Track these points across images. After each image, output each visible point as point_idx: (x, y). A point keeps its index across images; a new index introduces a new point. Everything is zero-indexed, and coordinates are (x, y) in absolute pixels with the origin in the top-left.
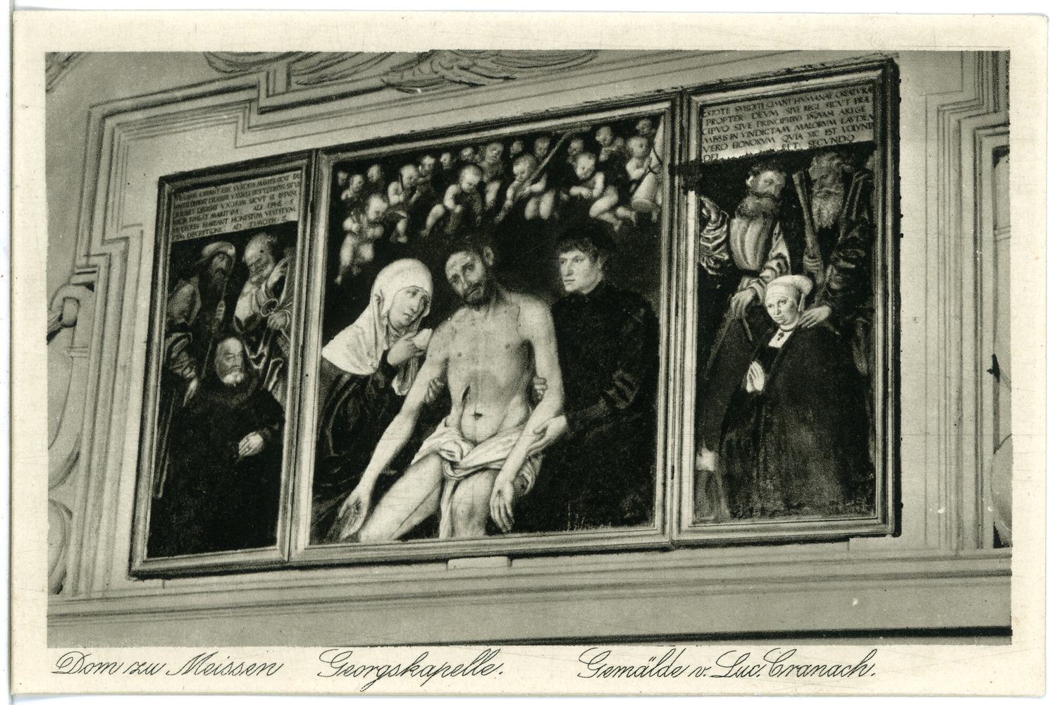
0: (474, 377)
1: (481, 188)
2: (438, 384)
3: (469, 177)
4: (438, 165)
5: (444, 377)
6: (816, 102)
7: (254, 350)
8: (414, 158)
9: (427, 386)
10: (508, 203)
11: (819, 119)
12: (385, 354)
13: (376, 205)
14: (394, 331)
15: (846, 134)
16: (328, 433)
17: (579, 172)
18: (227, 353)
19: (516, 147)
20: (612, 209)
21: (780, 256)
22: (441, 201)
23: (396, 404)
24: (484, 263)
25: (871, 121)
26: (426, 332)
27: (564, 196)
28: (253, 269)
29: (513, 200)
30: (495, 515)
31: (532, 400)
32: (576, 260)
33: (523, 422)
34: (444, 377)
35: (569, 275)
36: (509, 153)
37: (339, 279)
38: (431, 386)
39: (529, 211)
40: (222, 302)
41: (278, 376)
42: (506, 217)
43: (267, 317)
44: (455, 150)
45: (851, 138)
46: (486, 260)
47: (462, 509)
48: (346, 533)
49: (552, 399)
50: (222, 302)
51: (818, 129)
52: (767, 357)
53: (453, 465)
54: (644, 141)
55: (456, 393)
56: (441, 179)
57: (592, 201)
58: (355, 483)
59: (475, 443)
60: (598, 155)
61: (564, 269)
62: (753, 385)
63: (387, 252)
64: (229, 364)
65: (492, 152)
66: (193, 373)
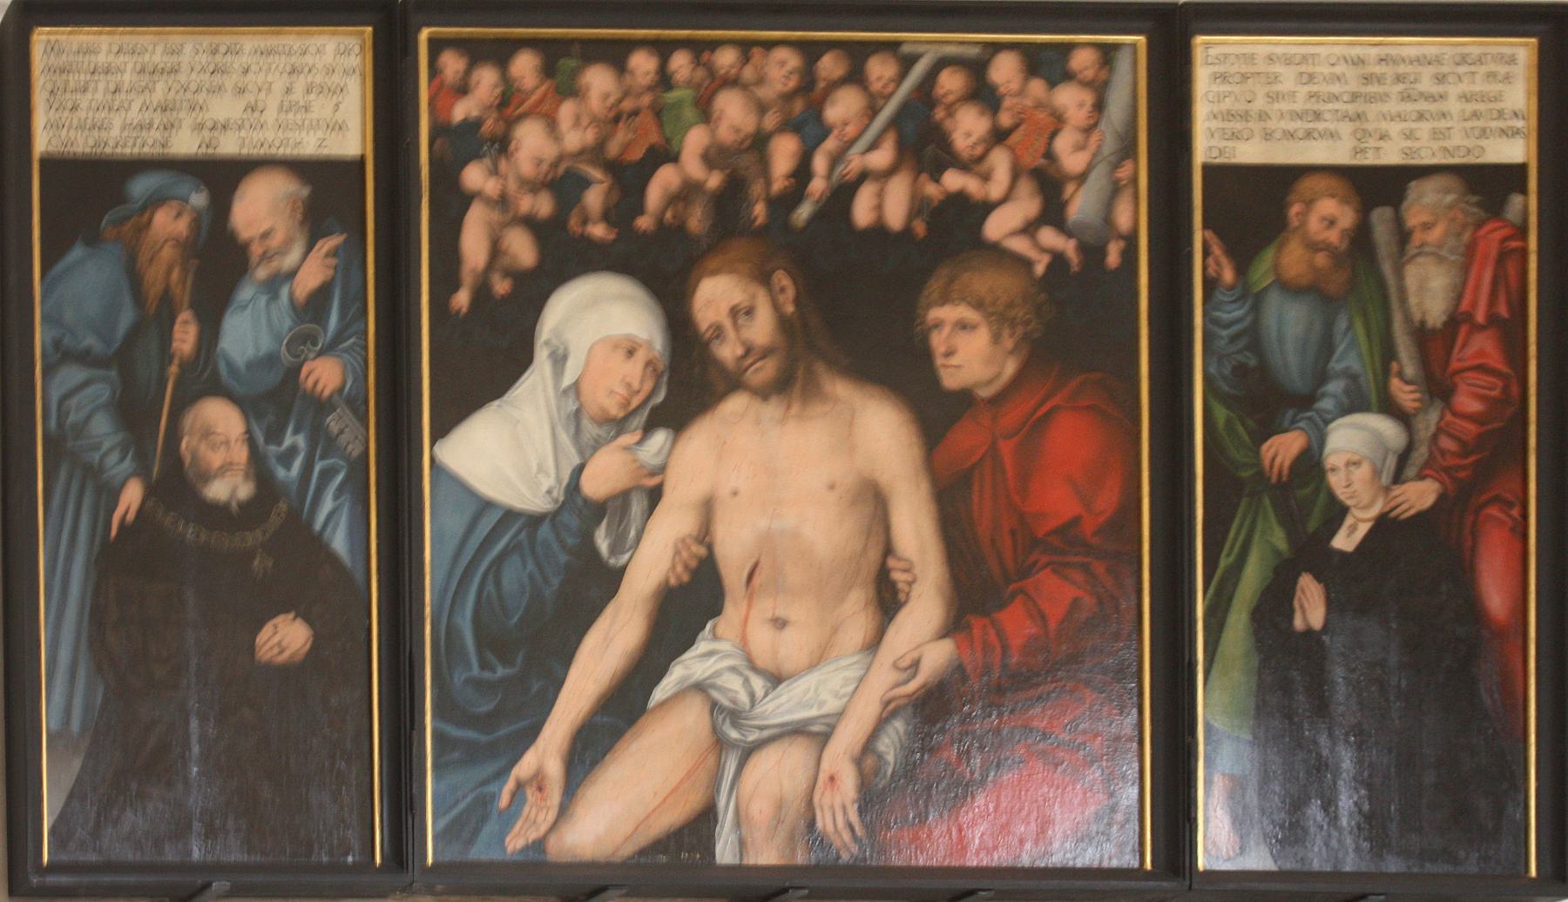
1: (759, 143)
3: (733, 112)
5: (705, 535)
7: (275, 435)
12: (579, 470)
19: (830, 66)
20: (1029, 229)
22: (673, 158)
23: (595, 584)
24: (776, 306)
26: (660, 438)
27: (931, 190)
28: (256, 250)
30: (824, 822)
31: (888, 599)
32: (963, 326)
34: (705, 535)
40: (185, 315)
41: (336, 498)
42: (817, 217)
46: (781, 298)
50: (185, 315)
53: (735, 716)
54: (1088, 98)
57: (988, 207)
59: (776, 679)
61: (938, 341)
63: (565, 257)
64: (216, 459)
66: (127, 465)
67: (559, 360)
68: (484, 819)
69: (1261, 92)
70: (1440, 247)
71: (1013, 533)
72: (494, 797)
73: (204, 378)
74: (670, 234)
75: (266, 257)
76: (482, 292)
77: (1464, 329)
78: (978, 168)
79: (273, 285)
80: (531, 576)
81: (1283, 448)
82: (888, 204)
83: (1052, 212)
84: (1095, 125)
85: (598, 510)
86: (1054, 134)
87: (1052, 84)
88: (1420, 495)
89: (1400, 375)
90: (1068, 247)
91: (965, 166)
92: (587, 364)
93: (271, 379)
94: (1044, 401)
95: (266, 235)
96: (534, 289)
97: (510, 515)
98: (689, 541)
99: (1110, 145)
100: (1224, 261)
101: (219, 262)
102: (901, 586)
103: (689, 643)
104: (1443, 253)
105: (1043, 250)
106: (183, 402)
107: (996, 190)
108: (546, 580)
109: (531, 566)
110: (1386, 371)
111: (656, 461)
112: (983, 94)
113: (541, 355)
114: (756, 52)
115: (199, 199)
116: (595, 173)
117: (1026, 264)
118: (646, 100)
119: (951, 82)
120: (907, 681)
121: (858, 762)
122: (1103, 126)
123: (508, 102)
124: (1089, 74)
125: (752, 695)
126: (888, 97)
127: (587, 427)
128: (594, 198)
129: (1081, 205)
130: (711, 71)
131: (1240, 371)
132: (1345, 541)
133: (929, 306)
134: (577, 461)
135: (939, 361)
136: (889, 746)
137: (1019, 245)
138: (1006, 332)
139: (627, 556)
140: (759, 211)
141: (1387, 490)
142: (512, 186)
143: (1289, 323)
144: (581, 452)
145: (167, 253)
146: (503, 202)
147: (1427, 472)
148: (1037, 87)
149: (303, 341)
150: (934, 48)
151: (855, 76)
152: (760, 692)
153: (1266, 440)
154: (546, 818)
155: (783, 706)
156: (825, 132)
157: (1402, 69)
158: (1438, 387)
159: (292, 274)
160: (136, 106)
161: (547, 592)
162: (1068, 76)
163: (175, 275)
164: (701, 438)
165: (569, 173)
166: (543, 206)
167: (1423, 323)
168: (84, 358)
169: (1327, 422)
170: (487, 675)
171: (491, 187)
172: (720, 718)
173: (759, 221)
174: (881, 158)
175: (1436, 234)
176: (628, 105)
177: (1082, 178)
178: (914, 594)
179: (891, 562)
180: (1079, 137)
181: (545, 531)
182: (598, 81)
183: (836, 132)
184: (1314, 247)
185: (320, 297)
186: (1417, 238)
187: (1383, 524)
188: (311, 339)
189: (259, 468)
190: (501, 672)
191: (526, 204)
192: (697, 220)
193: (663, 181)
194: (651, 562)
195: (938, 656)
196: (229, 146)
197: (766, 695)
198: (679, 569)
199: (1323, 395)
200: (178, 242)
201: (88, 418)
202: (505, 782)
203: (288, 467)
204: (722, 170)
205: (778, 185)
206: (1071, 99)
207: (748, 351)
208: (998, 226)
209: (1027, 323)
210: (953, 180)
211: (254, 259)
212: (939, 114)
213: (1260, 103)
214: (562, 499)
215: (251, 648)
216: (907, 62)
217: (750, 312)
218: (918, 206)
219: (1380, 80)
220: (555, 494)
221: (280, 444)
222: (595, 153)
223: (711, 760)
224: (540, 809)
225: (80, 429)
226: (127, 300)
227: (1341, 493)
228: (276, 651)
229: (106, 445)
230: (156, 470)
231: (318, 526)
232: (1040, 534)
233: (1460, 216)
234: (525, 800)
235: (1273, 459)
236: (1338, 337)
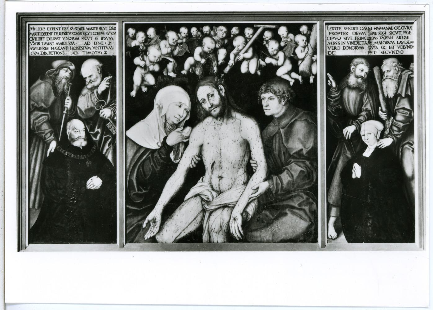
1: (215, 51)
2: (197, 158)
3: (208, 44)
4: (189, 33)
5: (200, 155)
6: (384, 30)
7: (92, 129)
8: (176, 28)
9: (191, 159)
11: (386, 40)
12: (165, 138)
13: (154, 53)
14: (170, 127)
15: (400, 50)
17: (270, 51)
19: (235, 30)
20: (289, 73)
21: (366, 110)
22: (192, 55)
23: (172, 168)
24: (220, 94)
26: (188, 129)
27: (262, 63)
28: (88, 80)
29: (234, 60)
30: (232, 231)
31: (250, 171)
32: (270, 98)
33: (246, 183)
34: (200, 155)
35: (267, 106)
36: (231, 34)
37: (133, 93)
38: (193, 159)
40: (68, 97)
41: (109, 145)
42: (230, 71)
43: (99, 111)
44: (199, 27)
45: (402, 52)
46: (221, 92)
48: (148, 236)
50: (68, 97)
51: (385, 45)
52: (362, 161)
53: (208, 202)
54: (305, 38)
56: (192, 43)
57: (277, 67)
59: (220, 192)
60: (279, 42)
61: (264, 103)
62: (355, 175)
63: (163, 80)
64: (76, 135)
65: (221, 32)
66: (52, 137)
67: (160, 108)
68: (139, 230)
69: (342, 37)
70: (392, 77)
71: (284, 153)
72: (142, 225)
73: (74, 114)
74: (191, 75)
75: (91, 82)
76: (139, 90)
77: (399, 98)
78: (275, 57)
79: (92, 90)
80: (152, 166)
81: (349, 130)
82: (250, 67)
83: (295, 68)
84: (307, 45)
85: (170, 148)
86: (296, 48)
87: (295, 35)
88: (387, 142)
89: (382, 110)
90: (299, 78)
91: (271, 57)
92: (168, 109)
93: (91, 114)
94: (292, 119)
95: (90, 76)
96: (153, 90)
97: (147, 150)
98: (195, 156)
99: (311, 51)
100: (333, 81)
101: (78, 83)
102: (253, 168)
103: (195, 183)
104: (393, 78)
105: (292, 78)
106: (68, 120)
107: (280, 63)
108: (156, 167)
109: (152, 164)
110: (378, 110)
111: (187, 135)
112: (276, 37)
113: (155, 107)
114: (214, 27)
115: (73, 67)
116: (171, 59)
117: (287, 82)
118: (184, 40)
119: (268, 35)
120: (256, 193)
121: (242, 214)
122: (309, 46)
123: (147, 41)
124: (305, 32)
125: (213, 197)
126: (250, 39)
127: (170, 127)
128: (170, 66)
129: (303, 67)
130: (202, 32)
131: (337, 110)
132: (367, 154)
133: (262, 93)
134: (165, 135)
135: (264, 108)
136: (251, 210)
137: (287, 77)
138: (283, 100)
139: (178, 161)
140: (215, 69)
141: (378, 140)
142: (148, 63)
143: (351, 97)
144: (167, 134)
145: (64, 81)
146: (145, 67)
147: (389, 136)
148: (291, 36)
149: (101, 104)
150: (264, 26)
151: (242, 33)
152: (215, 196)
153: (344, 128)
154: (157, 229)
155: (225, 199)
156: (233, 48)
157: (382, 30)
158: (391, 113)
159: (97, 87)
160: (55, 43)
161: (156, 170)
162: (300, 33)
163: (66, 87)
164: (199, 128)
165: (163, 59)
166: (156, 68)
167: (388, 96)
168: (40, 109)
169: (361, 123)
170: (140, 192)
171: (142, 63)
172: (204, 203)
173: (215, 72)
174: (249, 54)
175: (390, 74)
176: (180, 41)
177: (303, 60)
178: (257, 170)
179: (251, 161)
180: (302, 49)
181: (156, 154)
182: (172, 35)
183: (236, 48)
184: (357, 77)
185: (105, 93)
186: (386, 74)
187: (377, 149)
188: (102, 103)
189: (88, 137)
190: (144, 191)
191: (151, 68)
192: (198, 71)
193: (189, 61)
194: (185, 162)
195: (264, 186)
196: (81, 53)
197: (217, 197)
198: (193, 163)
199: (360, 116)
200: (67, 78)
201: (42, 124)
202: (145, 221)
203: (96, 138)
204: (205, 58)
205: (221, 62)
206: (300, 39)
207: (212, 106)
208: (280, 73)
209: (288, 98)
210: (268, 60)
211: (87, 83)
212: (265, 43)
213: (342, 40)
214: (161, 146)
215: (85, 185)
216: (255, 30)
217: (213, 95)
218: (259, 67)
219: (375, 33)
220: (159, 144)
221: (94, 131)
222: (171, 54)
223: (201, 215)
224: (154, 228)
225: (39, 128)
226: (52, 94)
227: (366, 142)
228: (92, 186)
229: (47, 131)
230: (60, 138)
231: (104, 153)
232: (292, 153)
233: (397, 68)
234: (150, 225)
235: (347, 133)
236: (364, 100)
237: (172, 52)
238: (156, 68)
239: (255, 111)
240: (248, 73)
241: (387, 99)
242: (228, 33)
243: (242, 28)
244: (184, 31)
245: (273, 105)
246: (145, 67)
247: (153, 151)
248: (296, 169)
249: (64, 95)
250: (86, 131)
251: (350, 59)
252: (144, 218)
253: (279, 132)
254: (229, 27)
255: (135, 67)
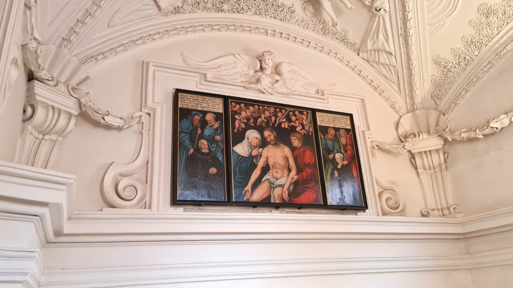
0: (275, 162)
1: (270, 117)
7: (211, 145)
10: (277, 122)
16: (237, 170)
18: (202, 144)
20: (301, 130)
23: (254, 166)
25: (237, 117)
28: (209, 122)
30: (284, 197)
31: (289, 171)
33: (288, 176)
34: (267, 161)
37: (236, 131)
39: (283, 126)
47: (276, 195)
49: (294, 172)
53: (272, 183)
55: (271, 166)
57: (296, 127)
58: (247, 185)
59: (277, 179)
61: (292, 141)
63: (248, 127)
64: (203, 147)
67: (248, 139)
73: (202, 137)
75: (210, 123)
76: (238, 130)
79: (211, 126)
81: (331, 156)
83: (303, 128)
85: (254, 157)
88: (346, 162)
93: (211, 138)
96: (245, 131)
101: (204, 123)
103: (266, 174)
113: (246, 138)
121: (288, 190)
127: (252, 147)
128: (251, 121)
132: (339, 167)
137: (300, 131)
146: (240, 120)
166: (245, 121)
168: (185, 133)
171: (239, 118)
174: (284, 120)
181: (247, 159)
182: (251, 108)
184: (331, 135)
185: (217, 128)
189: (209, 149)
191: (243, 120)
192: (264, 125)
193: (259, 120)
194: (261, 163)
195: (296, 177)
196: (205, 109)
200: (198, 120)
208: (298, 129)
210: (292, 124)
216: (286, 111)
218: (289, 126)
222: (251, 116)
225: (184, 142)
237: (252, 115)
238: (245, 121)
239: (289, 144)
240: (285, 128)
241: (343, 145)
242: (275, 111)
243: (281, 109)
244: (256, 107)
245: (296, 142)
246: (240, 120)
247: (246, 157)
248: (309, 171)
249: (197, 128)
250: (208, 145)
251: (327, 128)
252: (243, 190)
253: (300, 154)
254: (276, 108)
255: (236, 119)
